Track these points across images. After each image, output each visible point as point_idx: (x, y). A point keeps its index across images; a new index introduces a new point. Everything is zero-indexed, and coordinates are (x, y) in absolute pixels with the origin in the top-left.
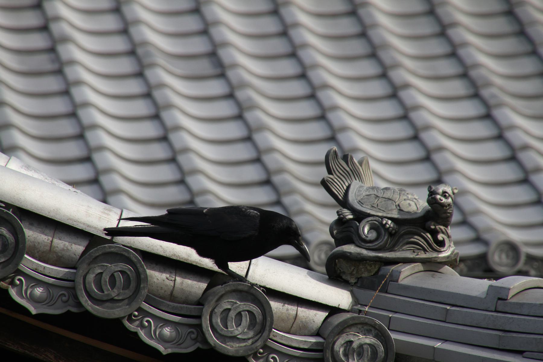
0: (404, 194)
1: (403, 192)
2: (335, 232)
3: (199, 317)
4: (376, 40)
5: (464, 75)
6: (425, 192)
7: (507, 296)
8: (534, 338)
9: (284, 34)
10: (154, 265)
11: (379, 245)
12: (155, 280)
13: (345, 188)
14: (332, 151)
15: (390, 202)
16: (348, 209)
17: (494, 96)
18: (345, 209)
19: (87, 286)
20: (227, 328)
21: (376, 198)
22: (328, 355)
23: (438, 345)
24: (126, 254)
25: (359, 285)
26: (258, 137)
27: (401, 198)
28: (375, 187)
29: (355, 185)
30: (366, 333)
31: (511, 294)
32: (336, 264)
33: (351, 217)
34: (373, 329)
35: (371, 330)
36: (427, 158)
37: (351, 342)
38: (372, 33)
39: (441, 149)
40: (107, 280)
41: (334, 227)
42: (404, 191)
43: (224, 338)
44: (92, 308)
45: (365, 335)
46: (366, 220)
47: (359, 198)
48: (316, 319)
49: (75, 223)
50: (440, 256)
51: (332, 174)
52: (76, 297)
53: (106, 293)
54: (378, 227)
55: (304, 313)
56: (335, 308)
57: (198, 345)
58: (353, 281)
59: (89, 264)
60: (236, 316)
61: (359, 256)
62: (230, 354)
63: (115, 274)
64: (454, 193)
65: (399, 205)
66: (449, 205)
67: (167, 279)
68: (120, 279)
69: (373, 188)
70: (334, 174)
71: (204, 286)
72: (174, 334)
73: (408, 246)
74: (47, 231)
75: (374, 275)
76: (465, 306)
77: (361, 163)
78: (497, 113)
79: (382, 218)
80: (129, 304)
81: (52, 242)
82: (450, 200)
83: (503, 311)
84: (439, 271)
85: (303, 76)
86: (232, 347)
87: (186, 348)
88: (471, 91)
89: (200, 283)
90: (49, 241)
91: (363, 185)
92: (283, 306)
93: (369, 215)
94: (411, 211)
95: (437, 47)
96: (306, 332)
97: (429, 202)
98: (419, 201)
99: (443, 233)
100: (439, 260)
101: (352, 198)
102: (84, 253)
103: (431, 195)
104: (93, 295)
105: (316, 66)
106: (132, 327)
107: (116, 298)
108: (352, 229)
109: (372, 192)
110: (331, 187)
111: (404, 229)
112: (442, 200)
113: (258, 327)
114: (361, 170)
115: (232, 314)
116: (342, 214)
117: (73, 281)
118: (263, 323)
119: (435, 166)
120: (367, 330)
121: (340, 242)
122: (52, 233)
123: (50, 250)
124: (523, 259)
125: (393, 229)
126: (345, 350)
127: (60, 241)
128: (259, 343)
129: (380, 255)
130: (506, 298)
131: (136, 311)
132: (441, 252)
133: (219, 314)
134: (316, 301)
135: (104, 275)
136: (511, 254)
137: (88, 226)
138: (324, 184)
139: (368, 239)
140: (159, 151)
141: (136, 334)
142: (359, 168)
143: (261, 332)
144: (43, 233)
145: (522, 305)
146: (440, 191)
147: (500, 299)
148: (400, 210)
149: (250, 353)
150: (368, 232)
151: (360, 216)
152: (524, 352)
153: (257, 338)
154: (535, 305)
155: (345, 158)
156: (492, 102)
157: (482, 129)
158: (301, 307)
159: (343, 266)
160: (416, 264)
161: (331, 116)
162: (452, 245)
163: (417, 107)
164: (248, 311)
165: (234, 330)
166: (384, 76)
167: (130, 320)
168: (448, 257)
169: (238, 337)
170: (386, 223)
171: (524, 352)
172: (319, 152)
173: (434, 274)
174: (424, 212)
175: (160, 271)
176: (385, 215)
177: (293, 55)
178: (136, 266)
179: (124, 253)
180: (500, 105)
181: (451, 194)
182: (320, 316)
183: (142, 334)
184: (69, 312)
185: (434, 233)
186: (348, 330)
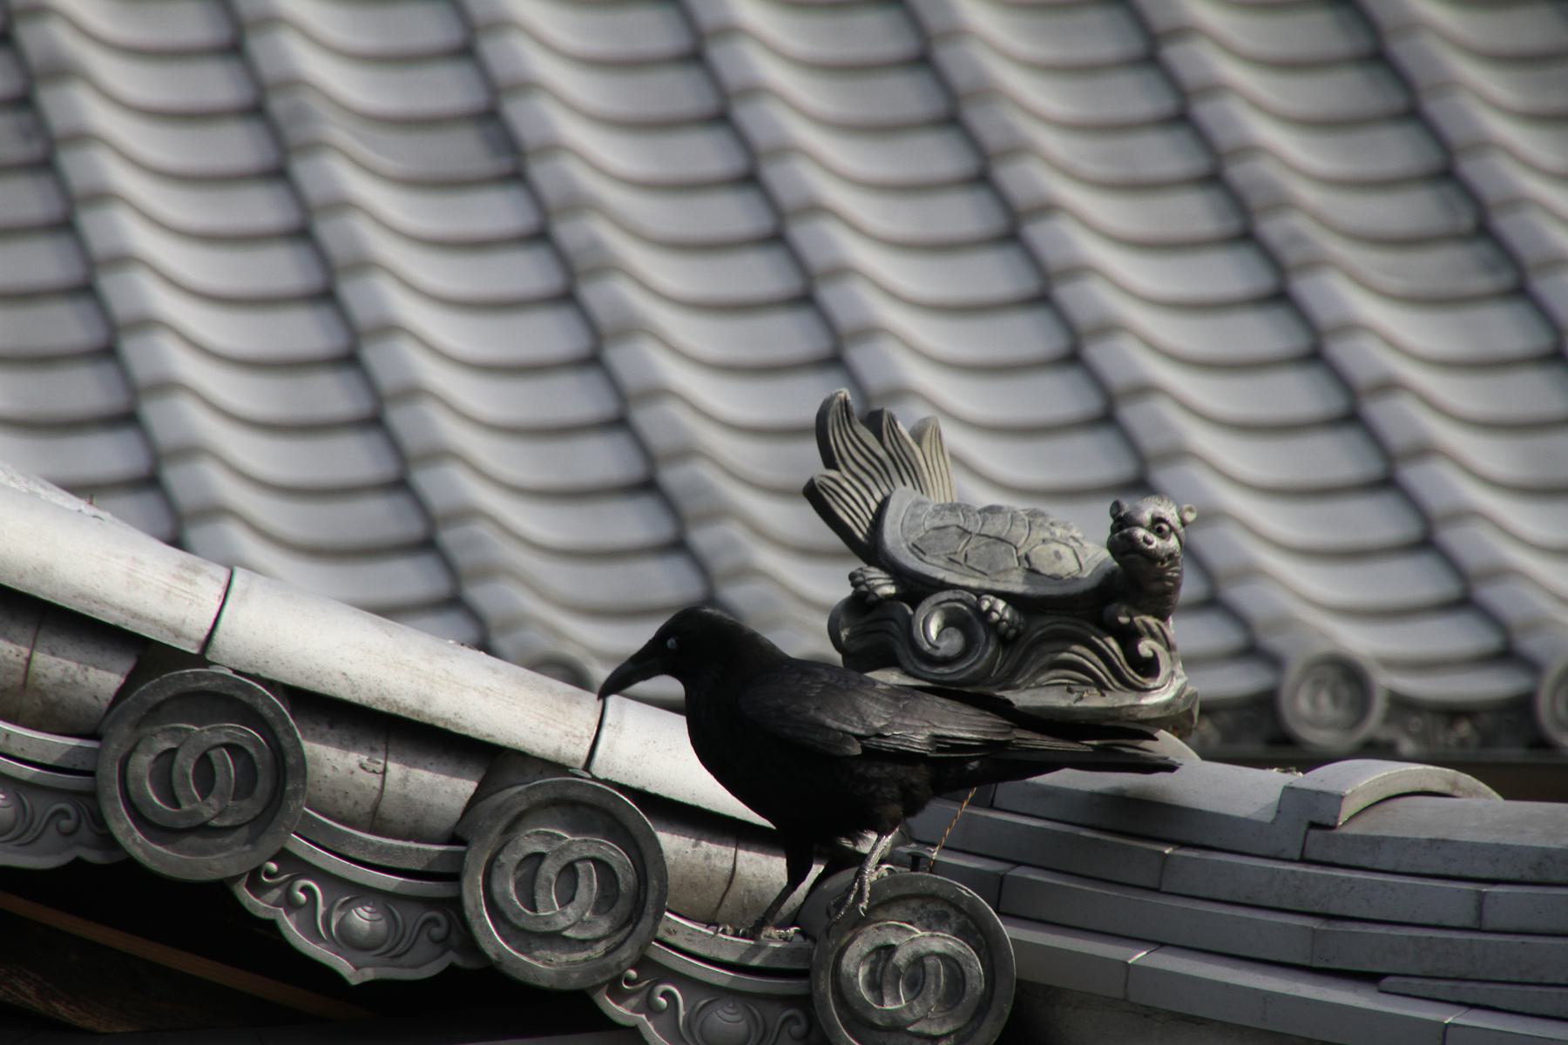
0: (1041, 525)
1: (1040, 520)
2: (844, 634)
3: (455, 877)
4: (960, 77)
5: (1213, 179)
7: (1336, 818)
10: (324, 729)
11: (971, 670)
12: (327, 771)
13: (874, 506)
14: (837, 401)
15: (1003, 548)
16: (882, 568)
17: (1297, 239)
18: (872, 569)
19: (132, 787)
20: (534, 909)
21: (961, 537)
22: (825, 985)
23: (1139, 956)
24: (245, 698)
26: (620, 357)
27: (1034, 535)
28: (959, 505)
29: (903, 498)
30: (934, 922)
31: (1347, 810)
33: (890, 590)
34: (952, 912)
35: (947, 916)
36: (1106, 418)
37: (890, 949)
38: (946, 55)
39: (1145, 390)
40: (190, 771)
41: (843, 619)
43: (524, 937)
44: (145, 850)
45: (929, 928)
47: (913, 537)
49: (95, 607)
50: (1144, 701)
51: (836, 468)
52: (99, 821)
53: (185, 807)
54: (968, 619)
57: (452, 958)
59: (137, 726)
60: (560, 874)
62: (544, 984)
63: (213, 754)
64: (1184, 523)
65: (1027, 558)
66: (1171, 556)
67: (362, 767)
68: (226, 767)
69: (953, 508)
70: (841, 466)
71: (467, 787)
72: (382, 925)
73: (1053, 673)
74: (16, 630)
77: (918, 436)
78: (1304, 287)
79: (980, 593)
80: (252, 841)
81: (29, 660)
82: (1173, 543)
83: (1324, 859)
85: (749, 180)
86: (548, 962)
87: (415, 967)
88: (1232, 225)
89: (455, 781)
90: (21, 660)
91: (924, 498)
92: (695, 846)
93: (942, 586)
94: (1063, 573)
95: (1135, 97)
97: (1112, 547)
98: (1086, 544)
99: (1153, 636)
100: (1140, 715)
101: (894, 537)
102: (122, 693)
105: (786, 150)
106: (260, 905)
107: (215, 823)
109: (950, 520)
110: (833, 505)
111: (1043, 625)
112: (1150, 543)
113: (622, 907)
115: (550, 869)
117: (91, 774)
119: (1129, 441)
120: (936, 915)
124: (1379, 706)
125: (1011, 624)
126: (872, 972)
127: (53, 660)
128: (627, 953)
131: (272, 860)
132: (1147, 690)
133: (510, 867)
135: (180, 756)
136: (1345, 693)
137: (135, 615)
138: (814, 495)
139: (938, 653)
140: (332, 396)
141: (272, 926)
142: (912, 450)
145: (1377, 842)
146: (1146, 516)
147: (1314, 825)
148: (1032, 571)
149: (600, 980)
150: (939, 634)
151: (916, 588)
153: (618, 937)
154: (1416, 842)
155: (875, 421)
156: (1291, 255)
157: (1262, 334)
158: (747, 849)
161: (830, 295)
163: (1078, 270)
164: (594, 860)
165: (555, 913)
166: (982, 179)
167: (255, 885)
168: (1167, 705)
169: (568, 933)
170: (991, 609)
172: (802, 399)
174: (1100, 577)
175: (341, 745)
176: (987, 585)
177: (721, 118)
178: (273, 732)
179: (238, 694)
180: (1315, 264)
181: (1178, 526)
183: (290, 926)
184: (78, 863)
185: (1128, 637)
186: (880, 914)
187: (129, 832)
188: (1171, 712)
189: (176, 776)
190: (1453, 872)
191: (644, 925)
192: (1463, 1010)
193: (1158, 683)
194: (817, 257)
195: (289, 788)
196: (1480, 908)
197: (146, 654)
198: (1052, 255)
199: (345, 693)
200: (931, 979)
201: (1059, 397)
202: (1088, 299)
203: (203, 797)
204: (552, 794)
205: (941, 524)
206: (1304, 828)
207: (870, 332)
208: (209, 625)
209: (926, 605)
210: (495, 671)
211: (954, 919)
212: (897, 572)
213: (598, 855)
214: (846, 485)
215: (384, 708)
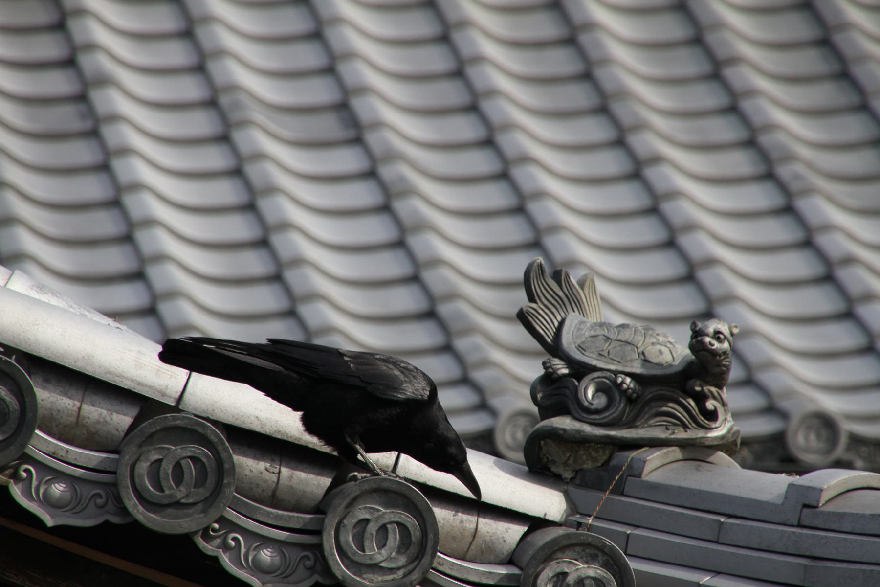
1: (650, 332)
2: (539, 396)
3: (318, 533)
5: (751, 143)
6: (685, 333)
7: (818, 502)
8: (861, 570)
9: (458, 74)
11: (611, 417)
12: (247, 472)
13: (556, 324)
14: (536, 264)
15: (629, 347)
16: (561, 359)
17: (798, 177)
18: (555, 359)
19: (137, 481)
20: (364, 551)
21: (606, 341)
24: (200, 430)
25: (577, 481)
27: (647, 341)
29: (573, 319)
30: (590, 559)
31: (825, 497)
32: (540, 448)
33: (565, 371)
34: (600, 554)
35: (597, 556)
36: (689, 278)
37: (564, 575)
38: (600, 73)
39: (711, 262)
40: (170, 472)
41: (539, 388)
42: (652, 329)
44: (145, 517)
45: (587, 562)
47: (579, 342)
48: (507, 537)
49: (117, 379)
51: (535, 302)
52: (118, 500)
53: (167, 492)
54: (610, 388)
55: (489, 527)
57: (316, 578)
58: (568, 475)
60: (378, 531)
61: (578, 436)
63: (183, 462)
64: (732, 334)
65: (643, 353)
66: (725, 353)
67: (267, 470)
68: (190, 469)
69: (602, 325)
70: (538, 301)
71: (326, 482)
72: (277, 560)
73: (658, 419)
74: (73, 392)
75: (602, 465)
76: (750, 516)
77: (582, 284)
78: (803, 204)
79: (616, 373)
80: (204, 511)
81: (80, 409)
82: (726, 345)
83: (812, 525)
84: (709, 460)
85: (488, 143)
86: (371, 581)
88: (761, 169)
89: (319, 478)
90: (75, 409)
91: (585, 319)
92: (454, 515)
93: (595, 369)
94: (663, 362)
95: (707, 97)
96: (492, 558)
97: (692, 347)
98: (677, 346)
99: (715, 398)
100: (707, 443)
101: (568, 341)
102: (132, 427)
104: (146, 495)
106: (209, 548)
107: (183, 501)
108: (567, 391)
109: (599, 332)
111: (652, 392)
112: (713, 345)
113: (413, 550)
114: (583, 296)
115: (372, 528)
116: (550, 367)
117: (114, 473)
119: (702, 291)
120: (591, 555)
121: (547, 411)
122: (80, 393)
123: (77, 422)
124: (843, 441)
125: (634, 391)
127: (93, 409)
128: (416, 576)
129: (613, 433)
130: (815, 505)
131: (216, 522)
132: (711, 429)
133: (350, 527)
134: (508, 507)
135: (164, 463)
136: (824, 433)
137: (139, 384)
138: (523, 318)
139: (593, 407)
141: (215, 559)
144: (65, 394)
145: (841, 516)
146: (711, 330)
147: (805, 506)
148: (646, 361)
150: (593, 396)
151: (580, 370)
154: (863, 516)
155: (557, 276)
156: (794, 186)
157: (778, 231)
158: (484, 518)
159: (552, 450)
160: (670, 449)
162: (729, 418)
163: (674, 194)
164: (398, 523)
166: (620, 142)
167: (206, 537)
168: (723, 437)
169: (382, 565)
170: (623, 382)
172: (515, 267)
173: (699, 466)
174: (684, 364)
175: (255, 458)
176: (620, 368)
180: (809, 191)
182: (516, 531)
183: (226, 560)
185: (701, 398)
186: (559, 555)
187: (135, 506)
188: (724, 441)
189: (162, 474)
191: (426, 560)
193: (717, 425)
194: (526, 186)
195: (225, 481)
197: (145, 405)
198: (659, 186)
199: (256, 427)
201: (663, 265)
202: (680, 211)
203: (177, 486)
204: (374, 486)
205: (595, 334)
206: (800, 507)
207: (556, 228)
208: (181, 390)
209: (586, 380)
213: (399, 520)
214: (541, 312)
215: (279, 437)
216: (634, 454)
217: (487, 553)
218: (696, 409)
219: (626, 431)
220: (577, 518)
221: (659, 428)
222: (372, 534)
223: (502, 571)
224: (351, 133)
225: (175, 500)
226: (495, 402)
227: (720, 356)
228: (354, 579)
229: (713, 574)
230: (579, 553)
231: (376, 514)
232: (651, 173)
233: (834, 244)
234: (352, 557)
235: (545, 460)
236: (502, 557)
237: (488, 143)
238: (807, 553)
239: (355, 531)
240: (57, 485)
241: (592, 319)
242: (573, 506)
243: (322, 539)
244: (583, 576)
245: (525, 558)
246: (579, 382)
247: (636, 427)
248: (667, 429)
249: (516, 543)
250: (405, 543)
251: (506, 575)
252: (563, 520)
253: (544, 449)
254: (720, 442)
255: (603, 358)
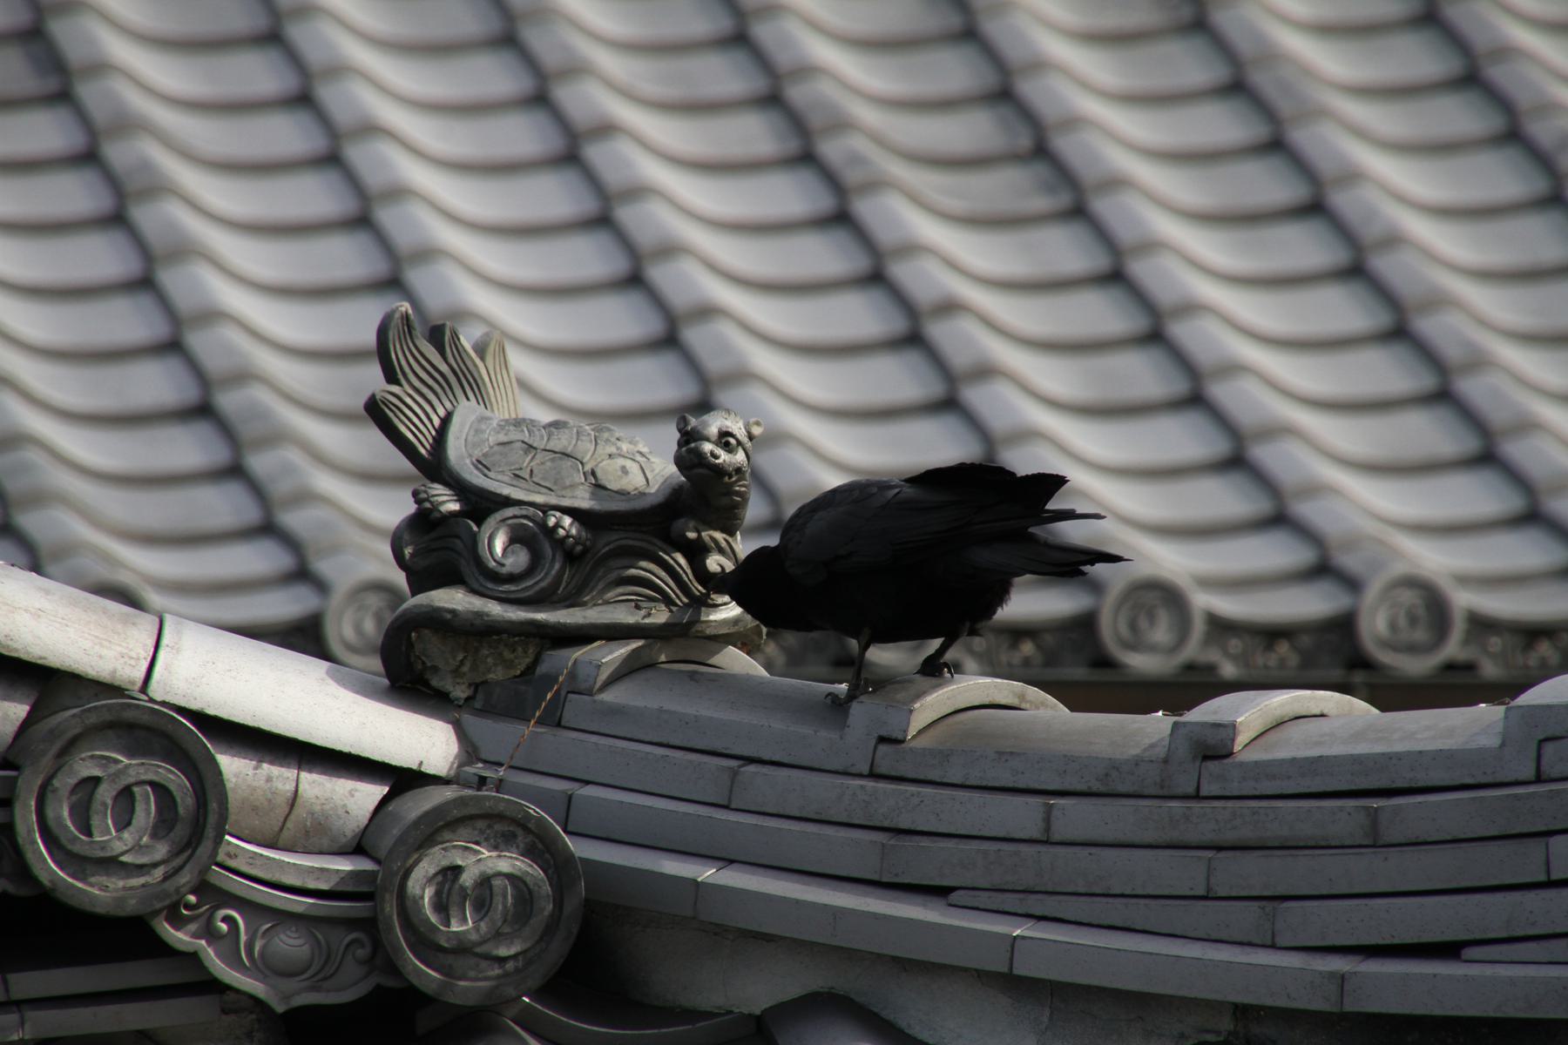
1: (606, 435)
2: (408, 551)
5: (772, 100)
6: (669, 436)
7: (905, 731)
11: (537, 588)
13: (437, 422)
14: (397, 315)
15: (569, 463)
17: (857, 160)
18: (436, 485)
20: (89, 834)
22: (390, 908)
23: (707, 873)
25: (478, 705)
27: (600, 449)
29: (466, 413)
30: (500, 843)
32: (411, 645)
34: (520, 832)
35: (514, 836)
36: (669, 341)
37: (456, 870)
39: (707, 312)
41: (406, 537)
42: (609, 430)
43: (80, 863)
45: (496, 848)
46: (499, 516)
47: (477, 453)
54: (534, 535)
55: (318, 787)
56: (409, 770)
58: (460, 692)
60: (115, 799)
61: (478, 622)
62: (100, 910)
64: (751, 437)
65: (593, 473)
66: (738, 470)
69: (518, 423)
71: (17, 711)
73: (621, 590)
75: (523, 674)
76: (786, 760)
77: (481, 350)
78: (865, 209)
79: (546, 509)
82: (740, 457)
84: (710, 662)
85: (303, 100)
86: (104, 888)
88: (792, 146)
91: (488, 413)
92: (256, 768)
93: (508, 502)
94: (630, 488)
96: (325, 843)
97: (679, 461)
99: (721, 551)
101: (457, 452)
103: (687, 442)
109: (514, 435)
111: (611, 540)
112: (717, 457)
113: (181, 832)
115: (106, 794)
116: (427, 500)
118: (198, 818)
119: (691, 362)
120: (503, 835)
121: (420, 581)
125: (578, 540)
126: (438, 894)
128: (185, 878)
129: (540, 616)
130: (900, 737)
131: (193, 892)
138: (376, 412)
139: (504, 570)
143: (192, 842)
146: (713, 430)
147: (883, 740)
148: (599, 486)
149: (158, 905)
150: (505, 550)
151: (480, 504)
152: (952, 889)
155: (437, 335)
156: (851, 176)
157: (823, 256)
158: (310, 771)
159: (432, 649)
163: (638, 192)
164: (152, 784)
165: (110, 838)
166: (540, 100)
169: (123, 859)
170: (558, 525)
171: (952, 889)
172: (359, 323)
174: (668, 491)
176: (553, 500)
180: (876, 185)
182: (365, 796)
185: (695, 553)
186: (447, 835)
190: (1021, 785)
192: (1031, 923)
194: (373, 179)
196: (1047, 820)
200: (498, 900)
201: (621, 319)
204: (108, 717)
205: (505, 439)
206: (873, 742)
207: (428, 254)
209: (492, 521)
210: (47, 592)
211: (522, 840)
212: (461, 488)
213: (155, 778)
214: (408, 400)
216: (578, 653)
217: (314, 835)
218: (689, 571)
219: (564, 612)
220: (478, 768)
221: (622, 607)
222: (104, 804)
223: (344, 865)
224: (51, 84)
225: (108, 854)
226: (324, 567)
227: (730, 476)
228: (72, 886)
229: (721, 864)
230: (482, 832)
231: (113, 768)
232: (596, 154)
233: (923, 279)
234: (70, 847)
235: (420, 667)
236: (344, 840)
237: (303, 100)
238: (886, 824)
239: (74, 798)
240: (283, 937)
241: (501, 412)
242: (469, 750)
243: (12, 815)
244: (490, 872)
245: (385, 844)
246: (479, 526)
247: (583, 604)
248: (638, 607)
249: (368, 816)
250: (166, 820)
251: (351, 872)
252: (452, 773)
253: (418, 648)
254: (732, 630)
255: (522, 483)
